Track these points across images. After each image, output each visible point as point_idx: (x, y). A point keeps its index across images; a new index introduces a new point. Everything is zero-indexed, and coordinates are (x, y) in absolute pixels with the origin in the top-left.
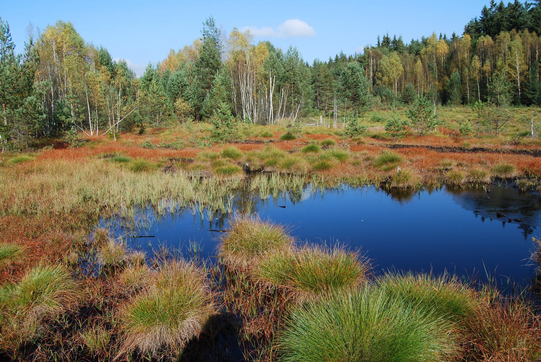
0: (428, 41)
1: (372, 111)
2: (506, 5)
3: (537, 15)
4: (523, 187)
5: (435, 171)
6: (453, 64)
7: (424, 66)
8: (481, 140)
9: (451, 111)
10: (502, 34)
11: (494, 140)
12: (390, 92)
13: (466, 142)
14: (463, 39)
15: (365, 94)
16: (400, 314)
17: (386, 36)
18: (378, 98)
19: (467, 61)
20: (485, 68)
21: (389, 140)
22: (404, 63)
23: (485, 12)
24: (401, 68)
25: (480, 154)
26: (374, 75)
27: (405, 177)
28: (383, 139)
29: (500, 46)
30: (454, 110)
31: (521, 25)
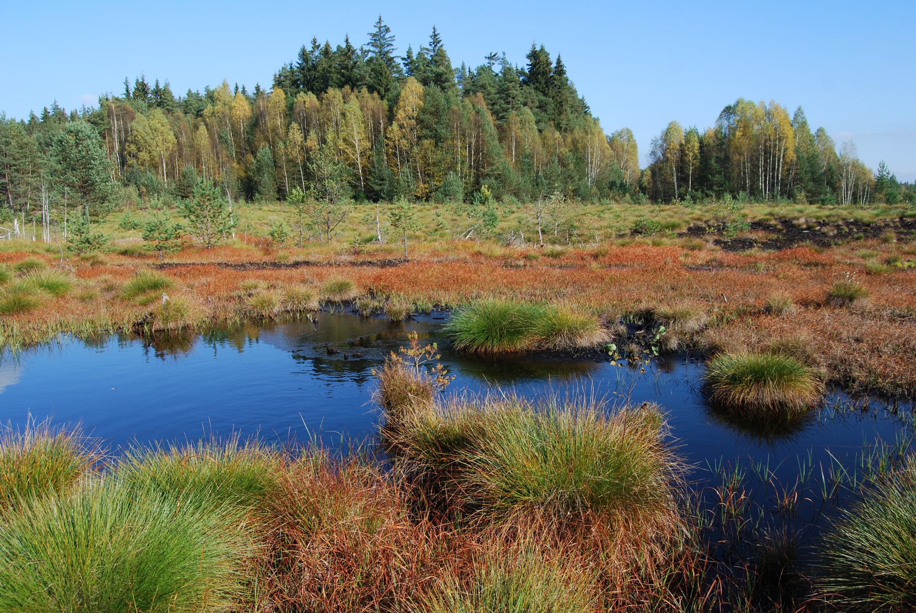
0: (216, 94)
1: (121, 211)
2: (334, 49)
3: (378, 67)
5: (230, 299)
6: (258, 135)
7: (211, 135)
8: (305, 249)
9: (260, 209)
10: (331, 91)
11: (325, 249)
12: (154, 178)
13: (281, 253)
14: (273, 96)
15: (106, 180)
16: (155, 515)
17: (141, 80)
18: (132, 189)
19: (281, 131)
20: (309, 143)
21: (151, 257)
22: (176, 129)
23: (304, 55)
24: (171, 137)
25: (304, 270)
26: (122, 149)
27: (178, 311)
28: (141, 256)
29: (328, 110)
30: (265, 208)
31: (357, 80)
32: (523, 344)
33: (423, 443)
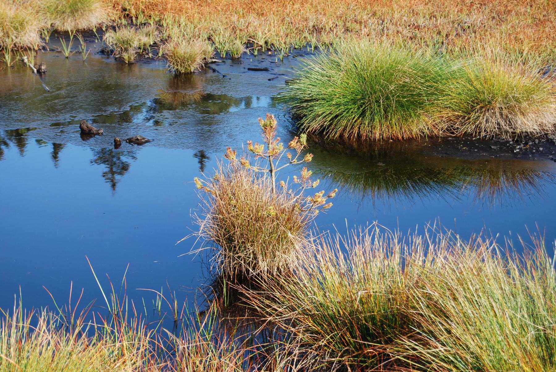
4: (126, 50)
32: (423, 124)
33: (326, 320)
